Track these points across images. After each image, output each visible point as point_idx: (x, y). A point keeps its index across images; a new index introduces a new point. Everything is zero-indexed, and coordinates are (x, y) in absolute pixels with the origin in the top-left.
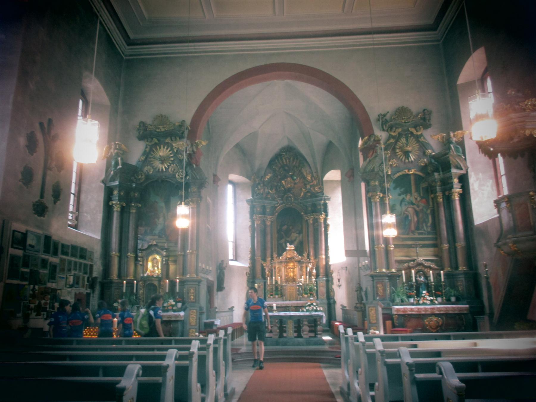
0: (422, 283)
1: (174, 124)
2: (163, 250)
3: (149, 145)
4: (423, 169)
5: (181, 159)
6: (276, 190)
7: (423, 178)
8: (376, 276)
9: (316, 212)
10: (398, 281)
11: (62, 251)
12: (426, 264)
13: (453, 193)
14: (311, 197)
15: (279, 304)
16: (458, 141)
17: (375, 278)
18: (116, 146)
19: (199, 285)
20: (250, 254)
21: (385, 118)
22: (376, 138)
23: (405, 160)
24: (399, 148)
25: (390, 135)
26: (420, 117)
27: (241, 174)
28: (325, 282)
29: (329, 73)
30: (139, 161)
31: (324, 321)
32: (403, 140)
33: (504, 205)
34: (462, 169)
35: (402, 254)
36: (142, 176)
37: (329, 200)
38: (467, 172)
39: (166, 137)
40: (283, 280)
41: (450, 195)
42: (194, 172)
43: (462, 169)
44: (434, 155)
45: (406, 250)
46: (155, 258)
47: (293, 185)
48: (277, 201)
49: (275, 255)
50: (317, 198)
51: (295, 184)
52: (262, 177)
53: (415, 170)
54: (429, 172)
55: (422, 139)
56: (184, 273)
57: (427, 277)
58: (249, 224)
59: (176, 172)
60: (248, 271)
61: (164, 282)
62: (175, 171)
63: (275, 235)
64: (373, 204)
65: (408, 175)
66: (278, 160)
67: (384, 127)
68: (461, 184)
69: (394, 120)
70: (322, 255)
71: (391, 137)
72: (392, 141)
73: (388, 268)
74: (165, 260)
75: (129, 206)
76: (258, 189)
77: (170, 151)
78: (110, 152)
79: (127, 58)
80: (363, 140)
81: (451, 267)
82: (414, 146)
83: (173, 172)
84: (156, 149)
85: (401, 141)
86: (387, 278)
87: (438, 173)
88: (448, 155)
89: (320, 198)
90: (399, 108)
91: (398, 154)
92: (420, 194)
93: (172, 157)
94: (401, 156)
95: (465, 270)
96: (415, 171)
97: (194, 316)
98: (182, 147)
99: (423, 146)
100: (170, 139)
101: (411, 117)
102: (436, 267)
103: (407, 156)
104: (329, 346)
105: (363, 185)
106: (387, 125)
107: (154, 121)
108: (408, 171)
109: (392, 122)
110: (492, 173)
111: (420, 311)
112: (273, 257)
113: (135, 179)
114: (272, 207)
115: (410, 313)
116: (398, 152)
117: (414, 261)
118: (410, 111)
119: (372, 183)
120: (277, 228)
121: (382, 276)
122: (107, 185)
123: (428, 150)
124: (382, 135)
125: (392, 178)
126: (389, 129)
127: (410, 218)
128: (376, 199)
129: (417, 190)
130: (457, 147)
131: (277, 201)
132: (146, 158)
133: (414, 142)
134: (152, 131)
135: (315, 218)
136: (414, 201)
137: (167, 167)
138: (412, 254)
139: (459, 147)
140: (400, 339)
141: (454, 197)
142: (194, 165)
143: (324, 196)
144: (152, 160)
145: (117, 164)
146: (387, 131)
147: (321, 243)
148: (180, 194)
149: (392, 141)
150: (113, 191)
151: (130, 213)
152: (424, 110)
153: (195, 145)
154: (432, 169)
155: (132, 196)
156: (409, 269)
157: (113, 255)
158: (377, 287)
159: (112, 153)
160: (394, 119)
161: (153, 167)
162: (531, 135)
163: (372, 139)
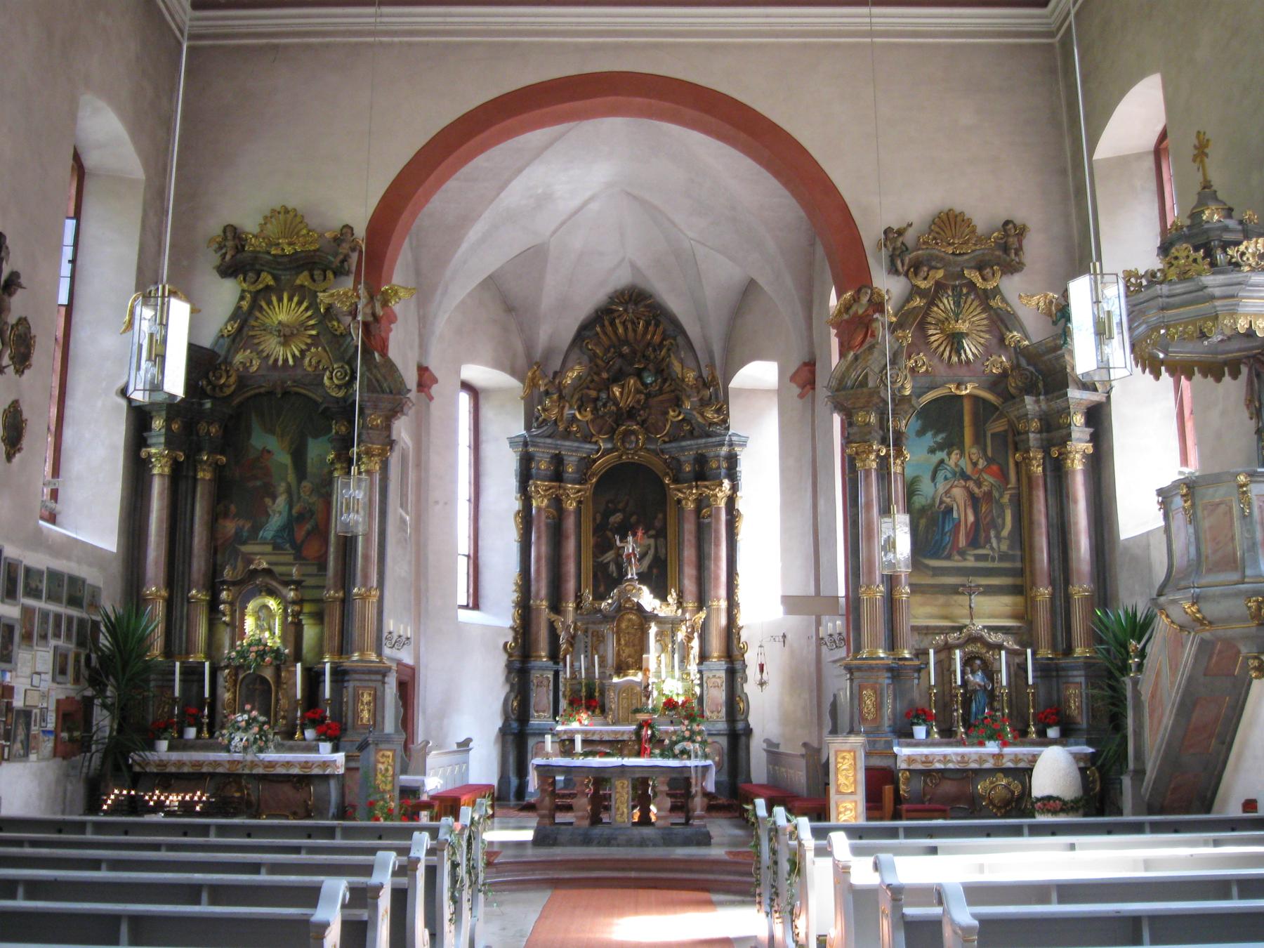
0: (978, 688)
1: (321, 236)
2: (286, 584)
3: (250, 292)
4: (997, 383)
5: (338, 333)
6: (595, 410)
7: (996, 408)
8: (859, 669)
9: (705, 479)
10: (916, 681)
11: (27, 585)
12: (994, 638)
13: (1070, 452)
14: (692, 435)
17: (856, 674)
19: (384, 683)
20: (515, 591)
21: (901, 239)
23: (950, 357)
25: (914, 286)
26: (995, 242)
27: (498, 365)
28: (723, 674)
32: (947, 302)
33: (1178, 502)
34: (1095, 390)
35: (929, 610)
36: (228, 377)
37: (743, 445)
38: (1108, 398)
39: (298, 269)
41: (1061, 458)
42: (375, 371)
45: (942, 599)
46: (266, 607)
48: (596, 443)
50: (710, 440)
51: (648, 396)
54: (1012, 391)
55: (996, 303)
56: (343, 649)
57: (990, 673)
58: (517, 505)
59: (325, 370)
60: (510, 638)
61: (289, 672)
62: (321, 367)
63: (589, 540)
64: (861, 475)
66: (603, 326)
68: (1091, 430)
69: (924, 247)
71: (915, 291)
72: (918, 302)
74: (293, 611)
76: (545, 410)
77: (307, 309)
80: (842, 300)
81: (1054, 647)
82: (975, 319)
84: (269, 303)
87: (1034, 398)
88: (1059, 352)
89: (718, 439)
91: (933, 339)
93: (313, 327)
94: (942, 343)
96: (974, 388)
98: (343, 302)
99: (1001, 321)
100: (308, 278)
102: (1018, 647)
104: (728, 849)
105: (837, 419)
106: (907, 261)
107: (265, 224)
109: (920, 252)
111: (967, 762)
113: (210, 387)
114: (582, 459)
115: (942, 766)
117: (960, 629)
118: (968, 222)
119: (860, 418)
120: (594, 519)
123: (1011, 332)
124: (889, 286)
125: (913, 406)
126: (912, 270)
127: (955, 515)
129: (979, 439)
131: (596, 443)
132: (240, 330)
133: (975, 309)
134: (259, 252)
135: (701, 494)
136: (969, 470)
137: (297, 353)
138: (957, 611)
140: (901, 832)
141: (1073, 461)
142: (376, 355)
143: (730, 433)
144: (258, 333)
146: (906, 275)
147: (718, 567)
148: (334, 431)
149: (918, 302)
150: (151, 418)
151: (195, 479)
152: (1007, 223)
154: (1020, 384)
155: (202, 432)
156: (948, 648)
157: (150, 595)
160: (925, 243)
161: (259, 353)
162: (1250, 334)
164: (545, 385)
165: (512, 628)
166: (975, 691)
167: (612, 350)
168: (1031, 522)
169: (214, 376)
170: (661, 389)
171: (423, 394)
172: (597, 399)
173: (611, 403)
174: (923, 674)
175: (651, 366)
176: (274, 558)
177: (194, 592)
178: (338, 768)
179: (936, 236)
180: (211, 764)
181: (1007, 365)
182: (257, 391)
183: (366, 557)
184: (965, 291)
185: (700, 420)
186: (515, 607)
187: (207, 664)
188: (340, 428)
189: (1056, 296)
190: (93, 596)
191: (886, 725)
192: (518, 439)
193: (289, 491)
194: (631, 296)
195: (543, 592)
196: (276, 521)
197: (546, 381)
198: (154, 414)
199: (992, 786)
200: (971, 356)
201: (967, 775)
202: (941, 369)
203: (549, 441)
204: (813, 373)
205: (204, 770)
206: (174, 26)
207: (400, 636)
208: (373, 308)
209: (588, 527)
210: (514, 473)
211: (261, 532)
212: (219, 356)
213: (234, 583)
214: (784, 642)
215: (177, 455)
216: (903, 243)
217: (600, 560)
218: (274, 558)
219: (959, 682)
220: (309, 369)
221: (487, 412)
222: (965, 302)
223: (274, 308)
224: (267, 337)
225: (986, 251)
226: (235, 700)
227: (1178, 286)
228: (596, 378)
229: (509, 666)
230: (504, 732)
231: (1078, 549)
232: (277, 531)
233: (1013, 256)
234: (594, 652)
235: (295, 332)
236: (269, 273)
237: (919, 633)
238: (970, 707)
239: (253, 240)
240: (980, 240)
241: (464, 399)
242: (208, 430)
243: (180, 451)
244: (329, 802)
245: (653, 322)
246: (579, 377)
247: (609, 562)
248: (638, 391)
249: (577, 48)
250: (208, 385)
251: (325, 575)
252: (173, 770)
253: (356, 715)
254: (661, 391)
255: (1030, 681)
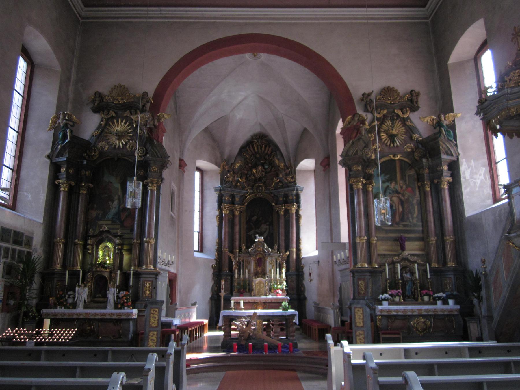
0: (409, 279)
1: (135, 96)
3: (105, 118)
6: (246, 178)
8: (357, 272)
12: (412, 259)
14: (282, 187)
15: (246, 300)
16: (449, 124)
17: (356, 274)
18: (65, 117)
19: (156, 279)
21: (369, 97)
22: (361, 118)
23: (390, 145)
24: (384, 132)
29: (310, 47)
30: (93, 136)
31: (296, 320)
32: (389, 123)
36: (95, 152)
37: (302, 190)
38: (458, 159)
39: (125, 110)
40: (480, 272)
41: (438, 183)
43: (452, 155)
44: (421, 140)
46: (107, 247)
47: (264, 173)
48: (247, 190)
49: (244, 247)
51: (266, 173)
52: (232, 164)
53: (402, 155)
55: (408, 123)
56: (140, 263)
58: (217, 213)
62: (134, 149)
63: (244, 226)
65: (394, 161)
66: (249, 148)
67: (369, 107)
69: (379, 101)
70: (293, 248)
73: (370, 263)
74: (118, 248)
75: (78, 186)
76: (227, 177)
77: (128, 126)
78: (58, 122)
79: (84, 20)
83: (132, 149)
84: (113, 123)
85: (386, 124)
86: (368, 274)
89: (292, 188)
90: (385, 88)
91: (383, 137)
92: (405, 181)
93: (131, 133)
94: (386, 140)
95: (454, 267)
97: (156, 316)
99: (411, 130)
100: (129, 113)
101: (397, 98)
103: (392, 140)
107: (112, 91)
108: (394, 156)
110: (485, 160)
112: (241, 249)
113: (87, 156)
114: (241, 196)
116: (383, 136)
118: (396, 91)
119: (355, 168)
120: (246, 218)
121: (362, 271)
122: (54, 161)
123: (415, 134)
128: (358, 186)
129: (403, 178)
130: (447, 131)
131: (247, 190)
132: (101, 134)
133: (399, 126)
134: (109, 102)
137: (124, 143)
139: (450, 130)
142: (155, 141)
144: (109, 135)
145: (65, 137)
151: (79, 193)
152: (412, 91)
153: (156, 117)
154: (419, 155)
156: (393, 264)
157: (56, 241)
158: (358, 285)
159: (59, 123)
161: (108, 143)
163: (356, 119)
164: (228, 168)
165: (215, 259)
166: (407, 281)
167: (253, 156)
168: (426, 211)
169: (89, 152)
170: (271, 170)
171: (181, 169)
172: (247, 174)
173: (252, 175)
174: (383, 274)
175: (267, 162)
176: (111, 227)
177: (77, 241)
178: (134, 316)
179: (383, 96)
180: (77, 314)
181: (413, 148)
182: (107, 158)
183: (150, 225)
184: (395, 118)
185: (286, 181)
186: (216, 251)
187: (81, 271)
188: (140, 173)
189: (435, 118)
190: (28, 241)
191: (370, 296)
192: (218, 188)
193: (119, 199)
194: (259, 137)
195: (227, 246)
196: (113, 211)
197: (228, 166)
198: (62, 166)
199: (417, 322)
200: (398, 144)
201: (406, 317)
202: (386, 150)
203: (229, 189)
204: (329, 161)
205: (74, 317)
206: (76, 12)
207: (169, 261)
208: (154, 122)
209: (244, 221)
210: (216, 201)
211: (107, 216)
212: (92, 144)
213: (94, 236)
214: (319, 264)
215: (71, 183)
216: (370, 99)
217: (248, 234)
218: (111, 227)
219: (400, 277)
220: (129, 149)
221: (206, 179)
222: (396, 123)
223: (115, 125)
224: (112, 137)
225: (404, 102)
226: (92, 286)
227: (515, 89)
228: (247, 166)
229: (214, 274)
230: (212, 299)
231: (448, 222)
232: (113, 216)
233: (415, 103)
234: (246, 268)
235: (123, 134)
236: (113, 111)
237: (381, 257)
238: (405, 288)
239: (107, 97)
240: (401, 98)
241: (197, 174)
242: (85, 173)
243: (73, 181)
244: (129, 331)
245: (268, 146)
246: (240, 166)
247: (251, 235)
248: (262, 171)
249: (239, 24)
250: (87, 155)
251: (133, 234)
252: (60, 317)
253: (144, 292)
254: (271, 171)
255: (429, 277)
